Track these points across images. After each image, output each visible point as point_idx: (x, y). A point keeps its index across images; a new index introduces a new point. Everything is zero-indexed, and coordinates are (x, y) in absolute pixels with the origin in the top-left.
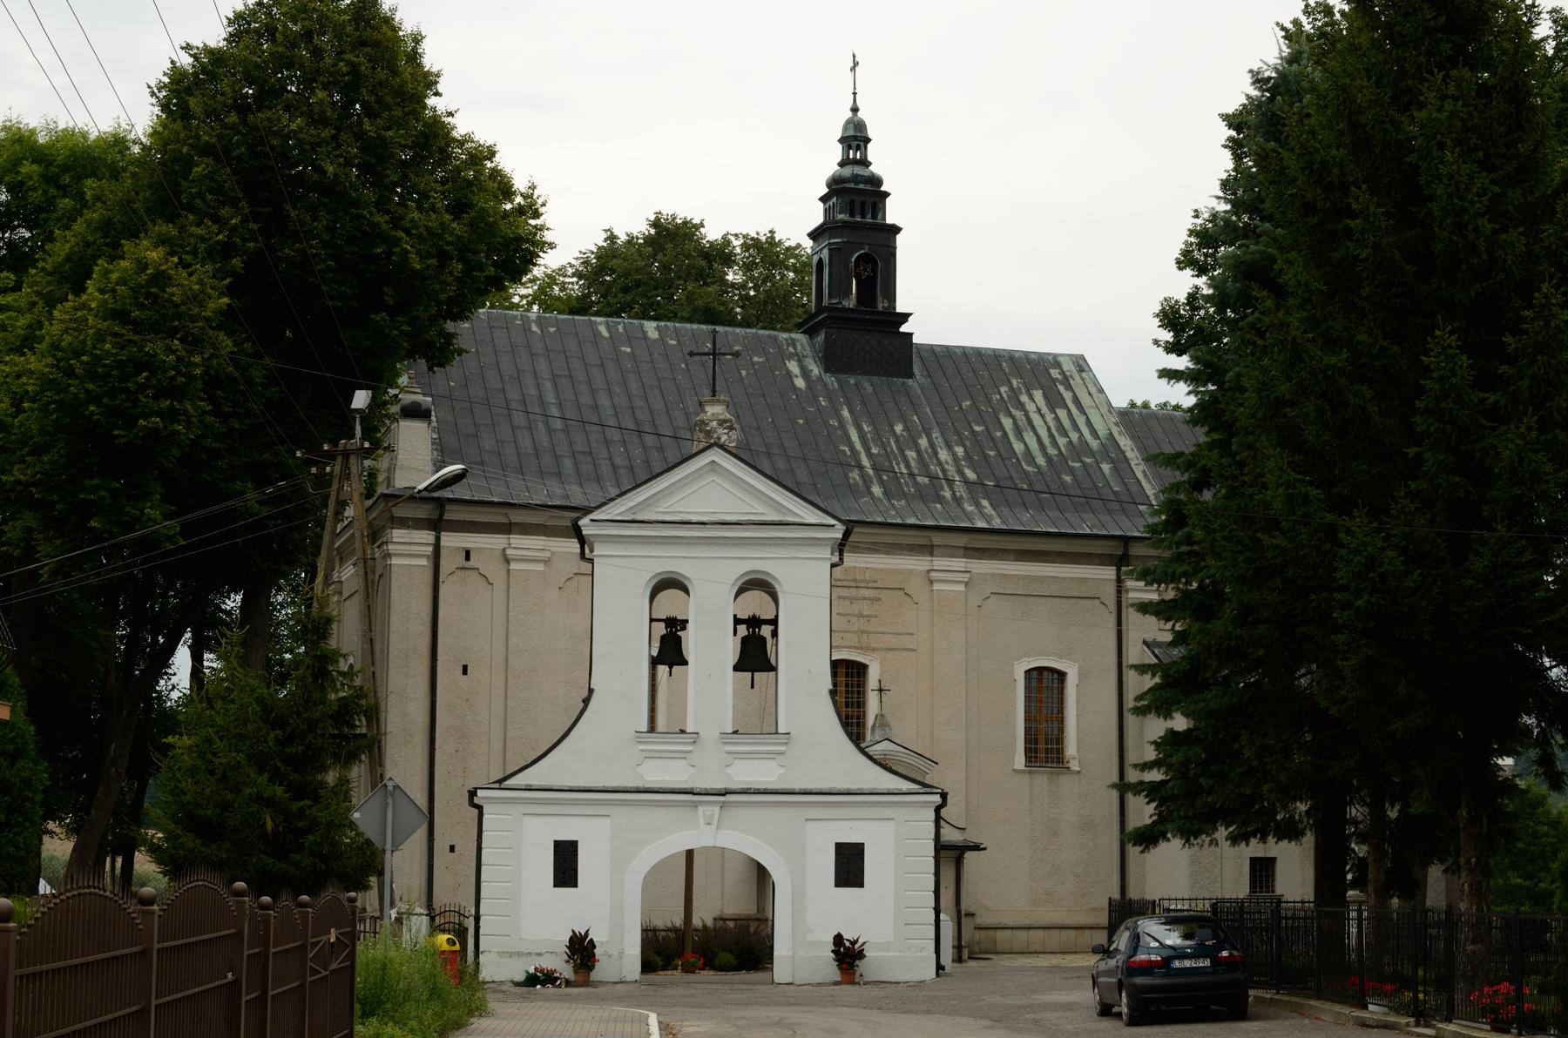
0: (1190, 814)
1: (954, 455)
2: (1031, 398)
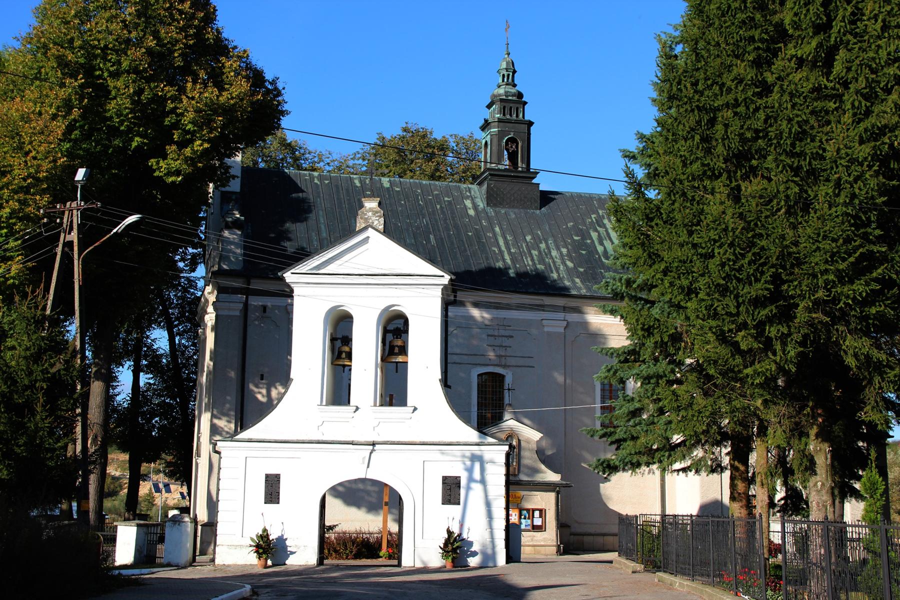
0: (633, 452)
1: (561, 253)
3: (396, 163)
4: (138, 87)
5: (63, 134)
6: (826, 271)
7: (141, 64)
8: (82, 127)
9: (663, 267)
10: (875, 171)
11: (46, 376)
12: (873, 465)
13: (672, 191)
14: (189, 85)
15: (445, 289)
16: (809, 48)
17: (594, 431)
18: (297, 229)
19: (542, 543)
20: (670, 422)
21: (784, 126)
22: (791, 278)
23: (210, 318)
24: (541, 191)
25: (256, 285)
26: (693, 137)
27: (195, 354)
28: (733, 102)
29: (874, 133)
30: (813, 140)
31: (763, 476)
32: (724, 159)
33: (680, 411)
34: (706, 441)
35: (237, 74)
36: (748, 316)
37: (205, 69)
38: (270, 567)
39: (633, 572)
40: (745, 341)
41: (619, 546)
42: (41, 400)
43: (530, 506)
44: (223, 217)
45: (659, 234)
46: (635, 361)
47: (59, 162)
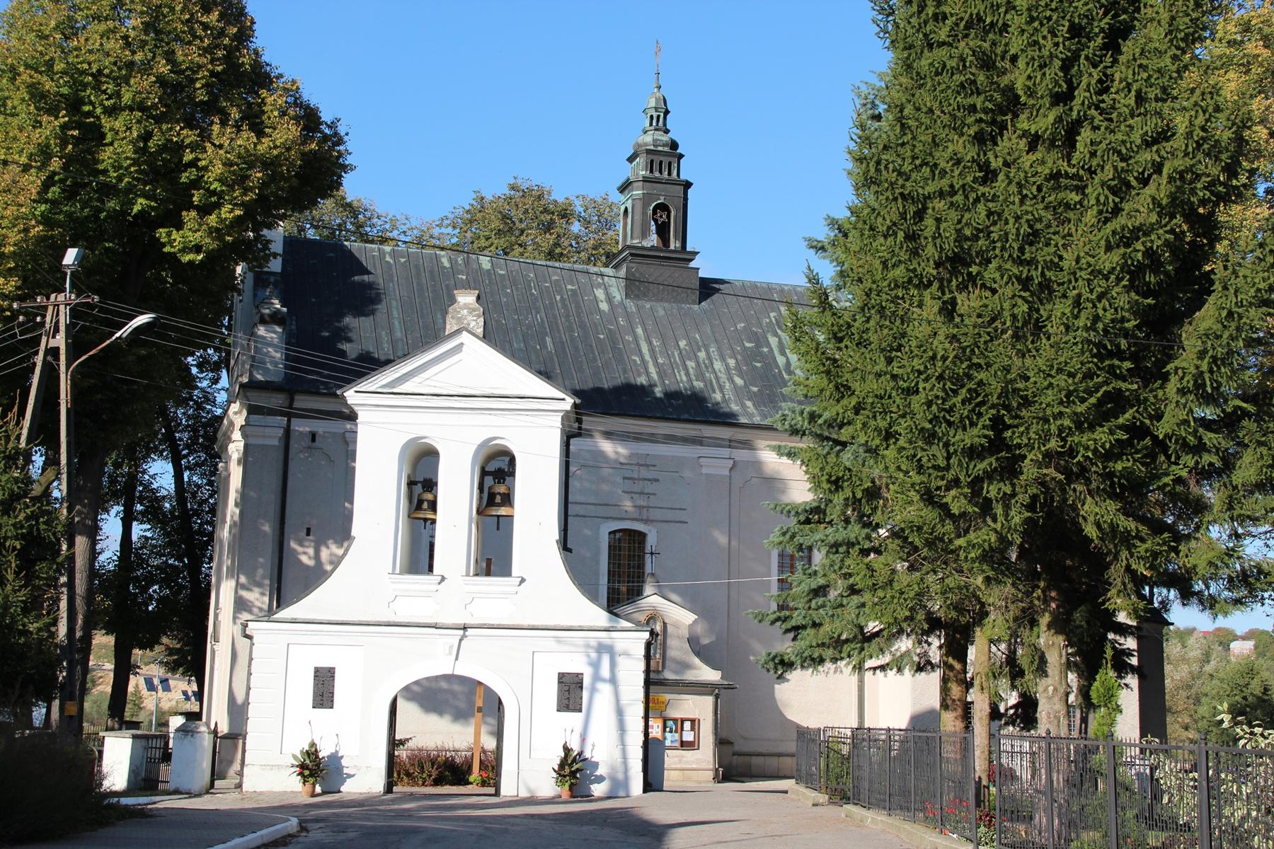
0: (814, 644)
1: (727, 366)
3: (499, 233)
5: (38, 193)
6: (1061, 414)
8: (62, 181)
9: (853, 403)
10: (1124, 286)
11: (19, 532)
12: (1109, 665)
13: (866, 305)
14: (216, 128)
15: (562, 417)
16: (1045, 122)
19: (694, 766)
20: (863, 605)
23: (236, 447)
25: (302, 402)
26: (895, 234)
27: (211, 496)
29: (1123, 236)
30: (1048, 245)
35: (283, 114)
36: (961, 471)
37: (238, 106)
38: (319, 795)
39: (814, 805)
40: (957, 502)
42: (13, 565)
44: (257, 307)
45: (850, 360)
46: (819, 522)
47: (33, 232)
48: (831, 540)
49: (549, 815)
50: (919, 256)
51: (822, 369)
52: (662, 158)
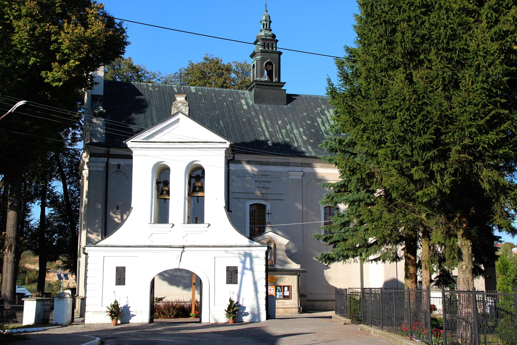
0: (344, 249)
1: (299, 131)
2: (329, 112)
3: (200, 79)
4: (33, 26)
6: (470, 126)
7: (34, 11)
9: (362, 127)
13: (368, 76)
14: (66, 25)
17: (319, 236)
18: (138, 117)
19: (290, 306)
20: (367, 230)
21: (442, 31)
22: (447, 131)
23: (85, 173)
24: (288, 95)
26: (381, 41)
27: (79, 195)
28: (407, 18)
31: (426, 262)
32: (402, 56)
33: (373, 222)
34: (389, 242)
36: (419, 157)
37: (76, 15)
38: (119, 324)
39: (345, 324)
40: (417, 174)
41: (336, 308)
43: (282, 284)
44: (92, 110)
46: (345, 191)
48: (351, 199)
49: (222, 332)
50: (393, 52)
51: (346, 111)
52: (269, 42)
